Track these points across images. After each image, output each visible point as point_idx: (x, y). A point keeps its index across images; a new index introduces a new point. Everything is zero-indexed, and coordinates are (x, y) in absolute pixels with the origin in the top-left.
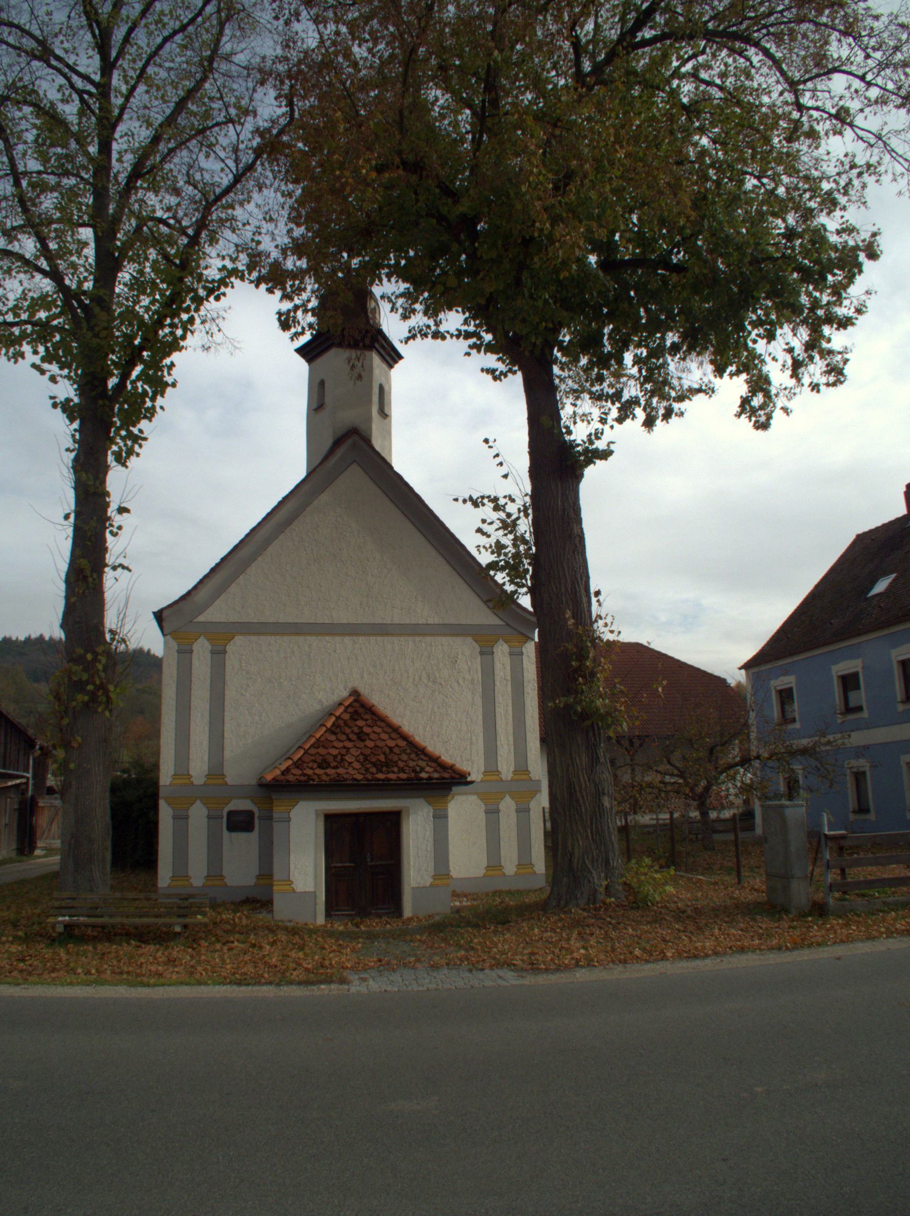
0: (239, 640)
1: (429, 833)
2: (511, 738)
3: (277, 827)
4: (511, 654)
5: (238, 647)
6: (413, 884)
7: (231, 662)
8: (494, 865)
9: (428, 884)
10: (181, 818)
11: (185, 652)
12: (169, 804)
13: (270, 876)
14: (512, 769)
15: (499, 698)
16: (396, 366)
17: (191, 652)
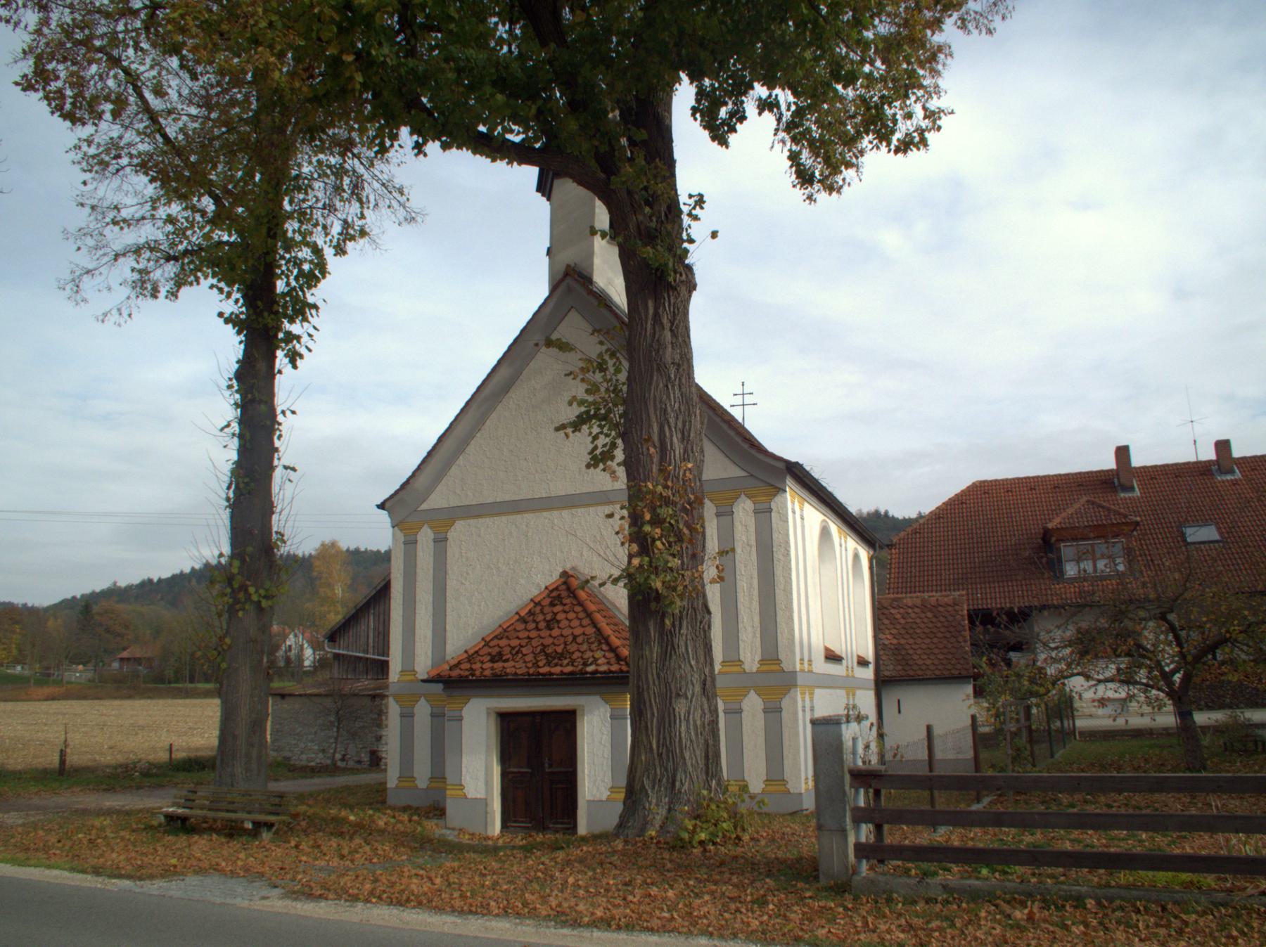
0: (459, 525)
1: (606, 739)
2: (757, 619)
4: (756, 512)
5: (459, 532)
6: (588, 796)
7: (452, 549)
9: (604, 798)
10: (407, 716)
11: (410, 543)
13: (443, 778)
14: (758, 658)
17: (416, 542)
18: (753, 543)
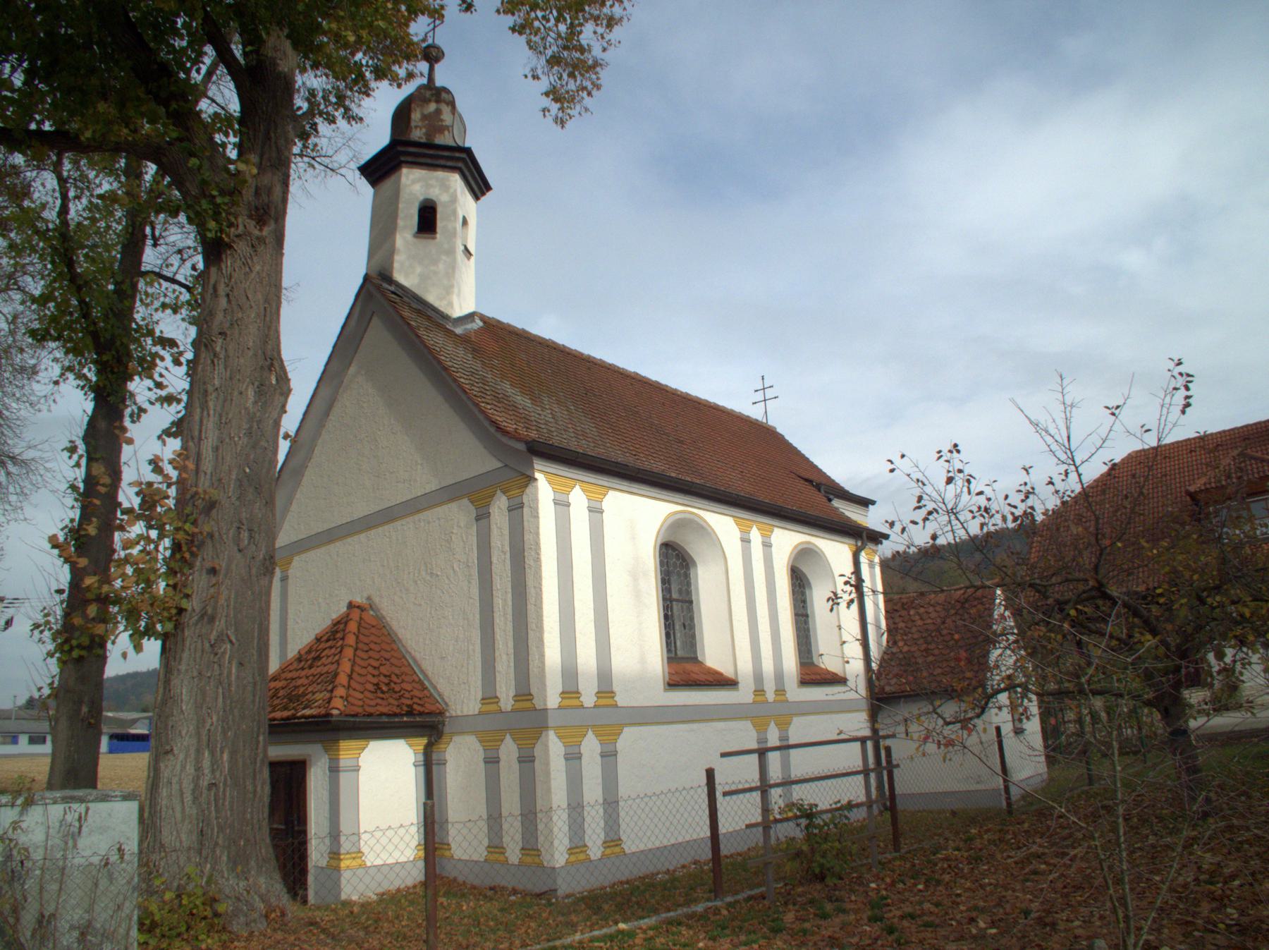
2: (511, 644)
3: (343, 777)
8: (496, 847)
12: (514, 740)
14: (512, 693)
15: (496, 579)
16: (483, 199)
18: (507, 548)
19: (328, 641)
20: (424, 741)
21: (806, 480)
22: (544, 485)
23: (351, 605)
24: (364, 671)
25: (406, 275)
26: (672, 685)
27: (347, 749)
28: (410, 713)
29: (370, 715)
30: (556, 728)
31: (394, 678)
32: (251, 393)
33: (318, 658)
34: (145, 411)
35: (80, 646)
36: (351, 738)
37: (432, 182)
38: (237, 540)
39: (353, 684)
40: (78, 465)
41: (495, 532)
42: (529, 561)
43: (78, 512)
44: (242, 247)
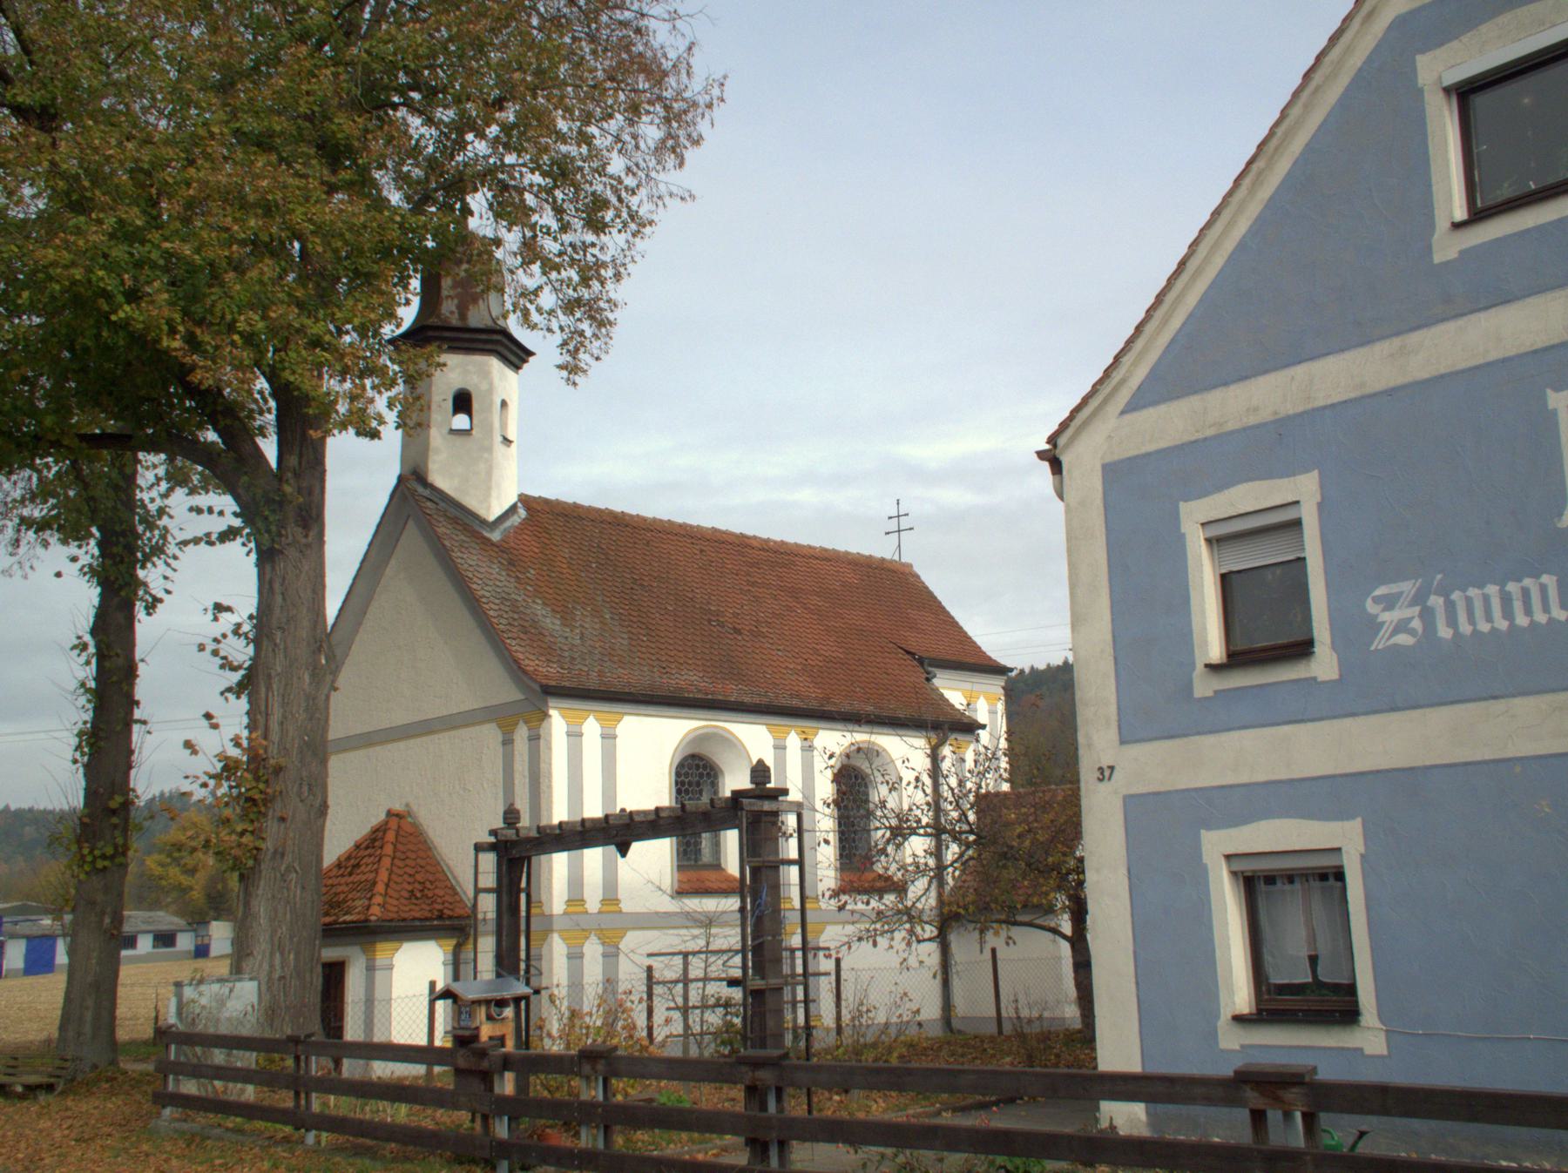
16: (525, 366)
19: (367, 848)
20: (453, 942)
21: (908, 652)
22: (557, 721)
23: (390, 813)
24: (399, 880)
25: (441, 478)
26: (680, 893)
27: (382, 950)
28: (440, 917)
29: (404, 920)
30: (560, 931)
31: (428, 885)
32: (307, 677)
33: (357, 866)
34: (161, 601)
35: (104, 857)
36: (386, 940)
37: (470, 368)
38: (299, 794)
39: (390, 891)
40: (88, 663)
41: (517, 758)
42: (543, 787)
43: (91, 713)
44: (292, 553)
